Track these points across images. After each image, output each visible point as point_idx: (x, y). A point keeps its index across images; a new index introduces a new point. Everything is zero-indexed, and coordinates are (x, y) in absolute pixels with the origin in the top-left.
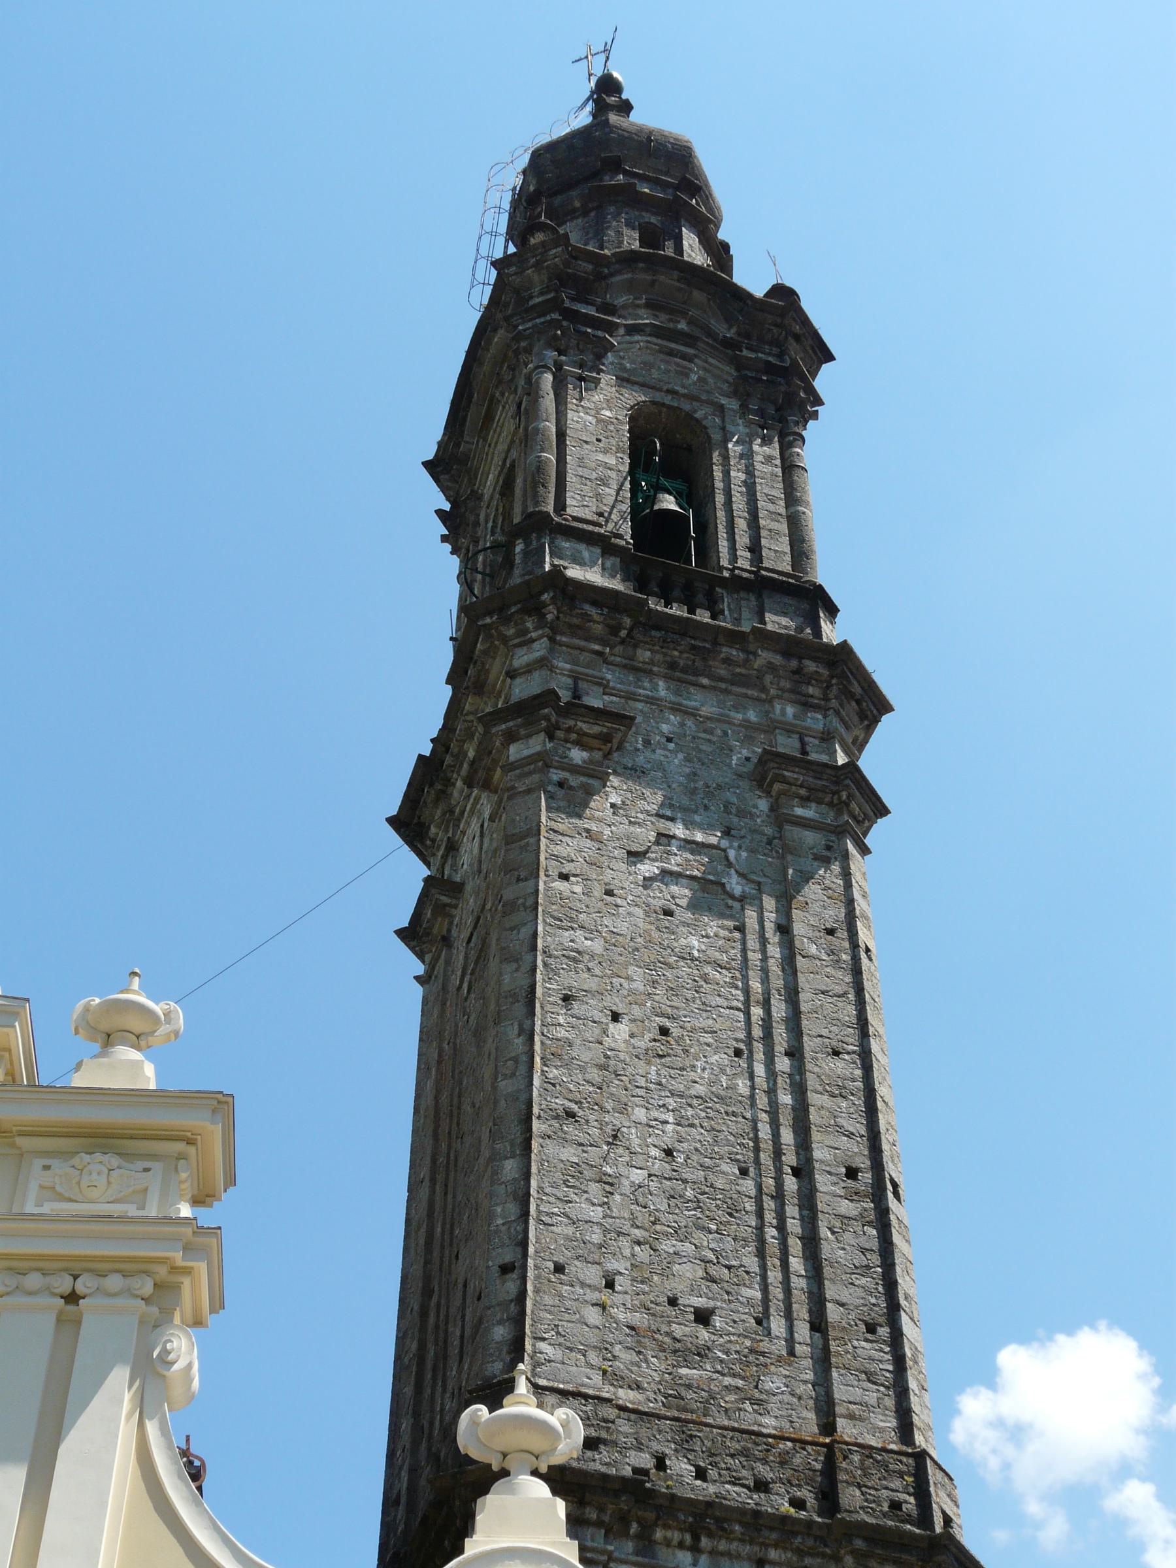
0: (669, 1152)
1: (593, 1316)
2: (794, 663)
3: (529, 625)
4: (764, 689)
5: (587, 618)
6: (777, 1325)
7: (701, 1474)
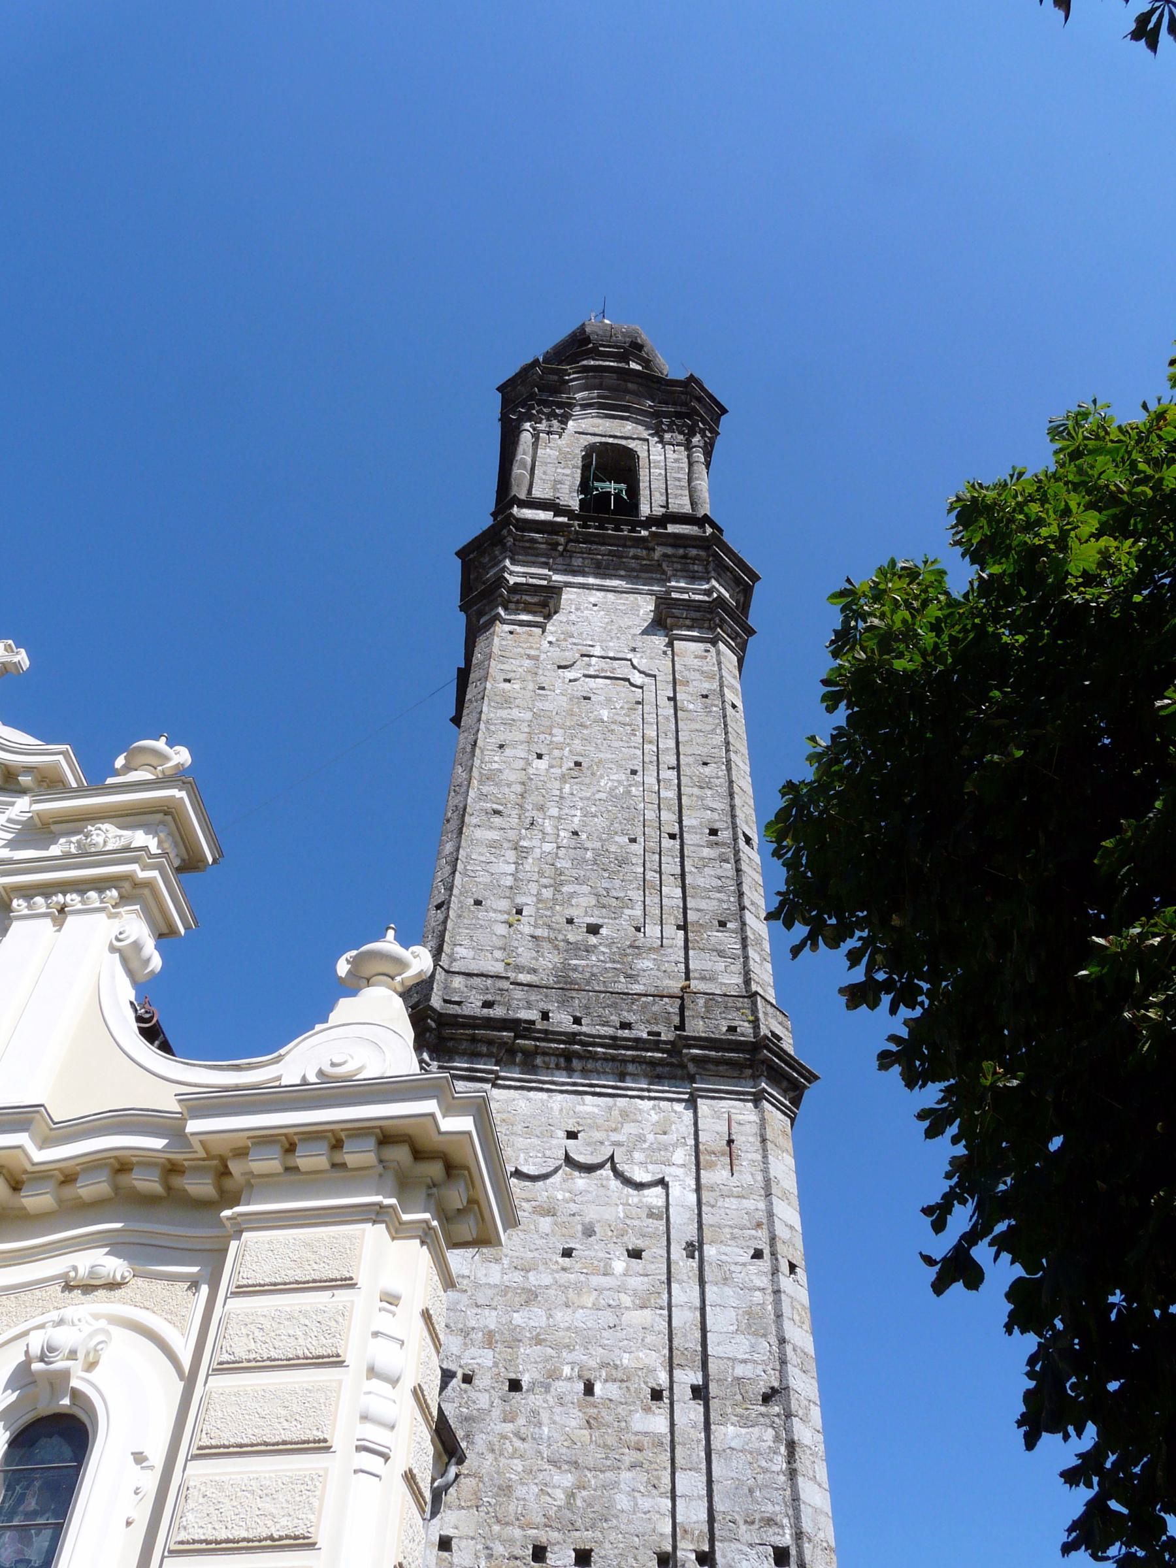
1: (502, 929)
2: (681, 551)
7: (577, 1021)
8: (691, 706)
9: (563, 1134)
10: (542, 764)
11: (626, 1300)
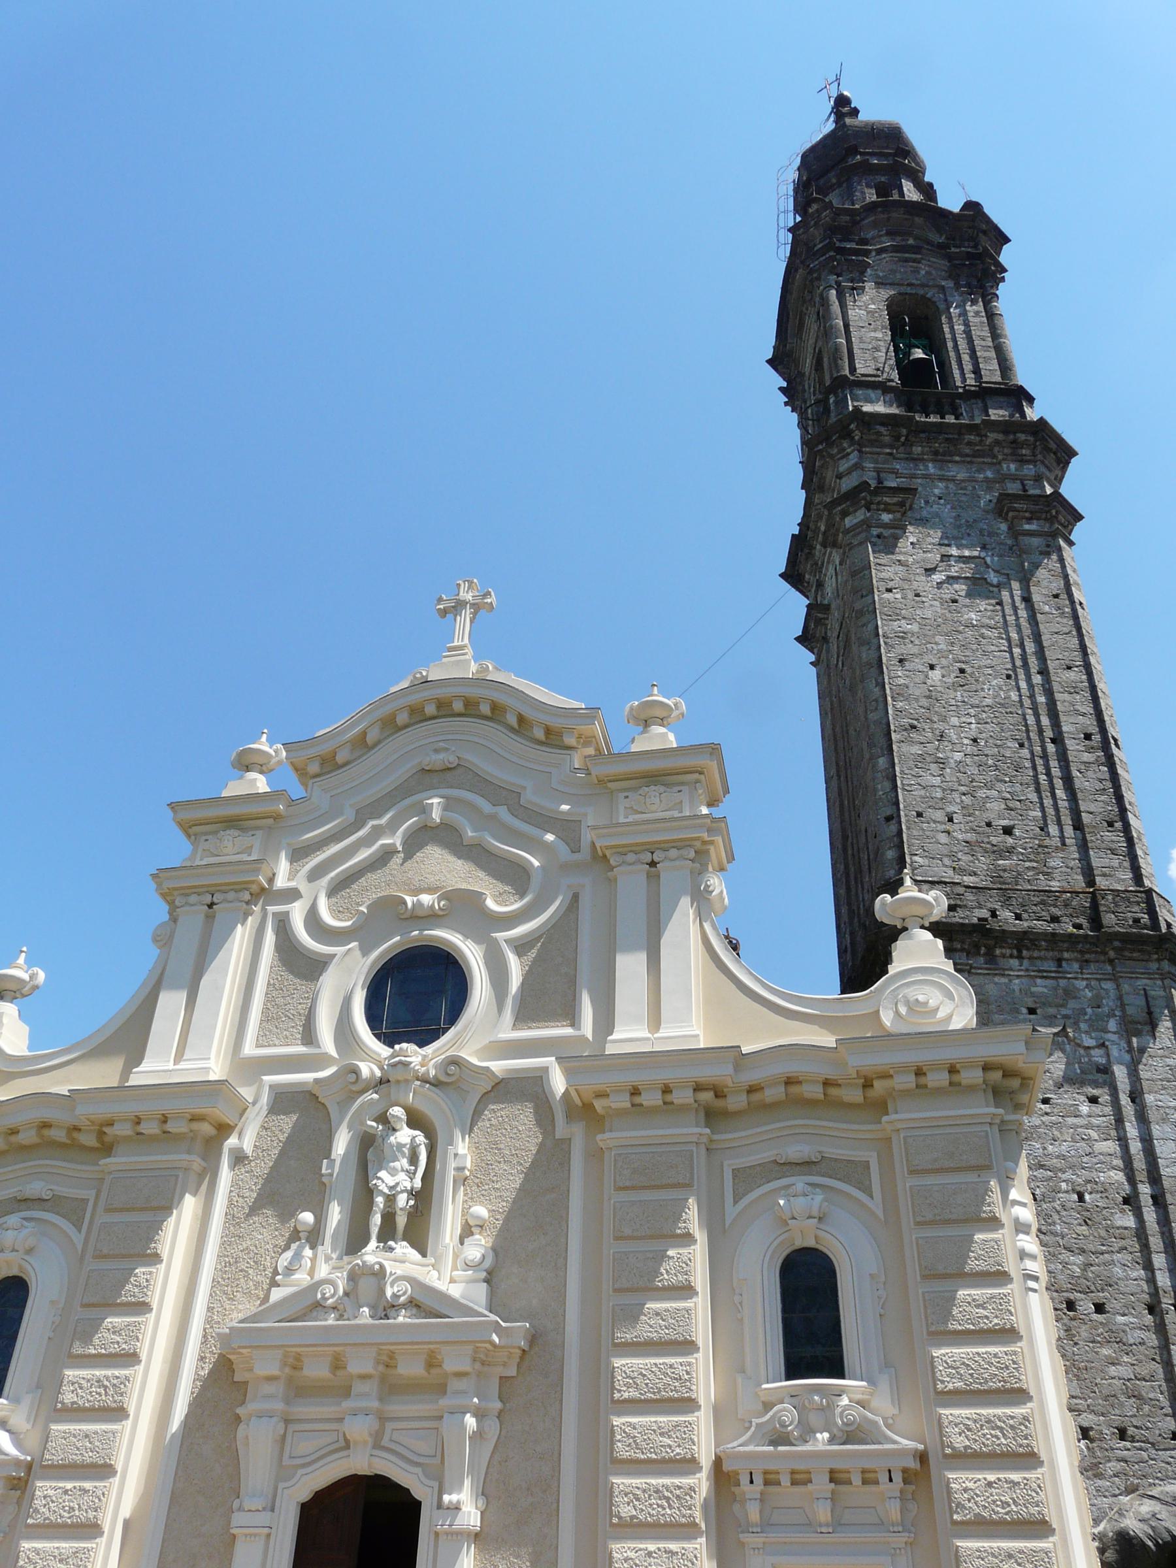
0: (975, 740)
1: (943, 838)
3: (845, 445)
4: (995, 457)
5: (879, 434)
6: (1053, 830)
8: (1047, 608)
9: (1025, 1011)
10: (936, 675)
11: (1094, 1135)
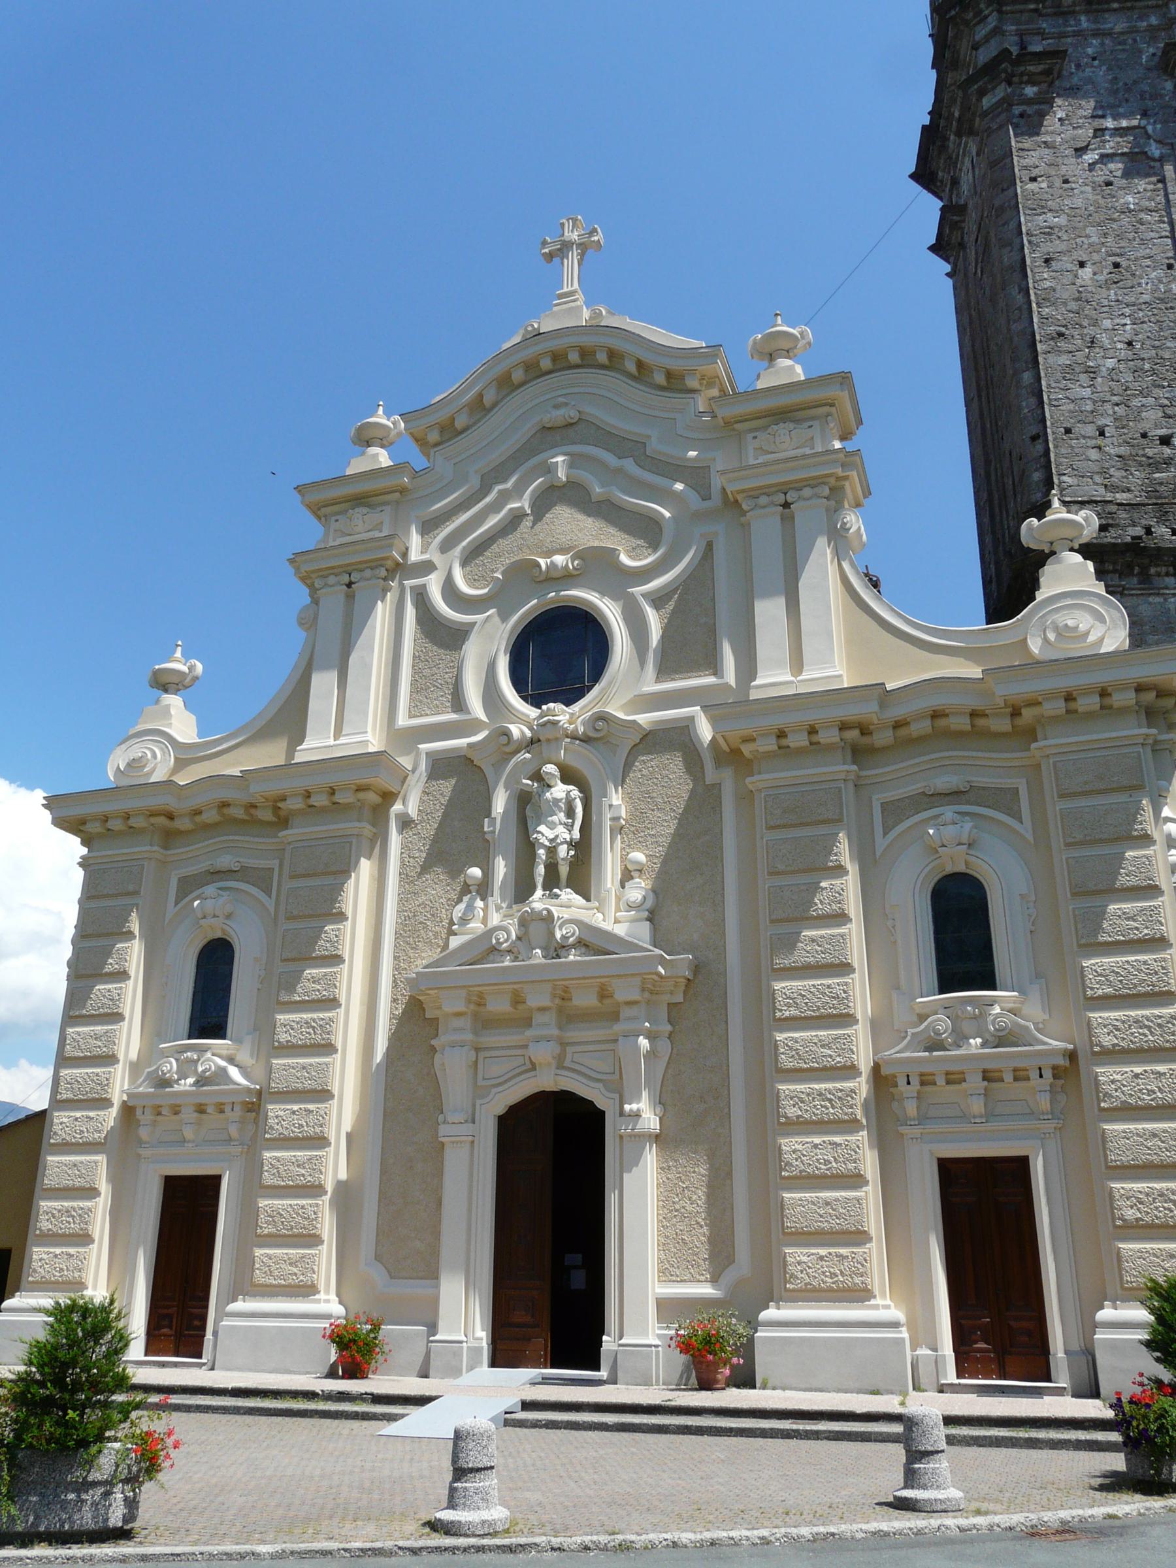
1: (1094, 454)
